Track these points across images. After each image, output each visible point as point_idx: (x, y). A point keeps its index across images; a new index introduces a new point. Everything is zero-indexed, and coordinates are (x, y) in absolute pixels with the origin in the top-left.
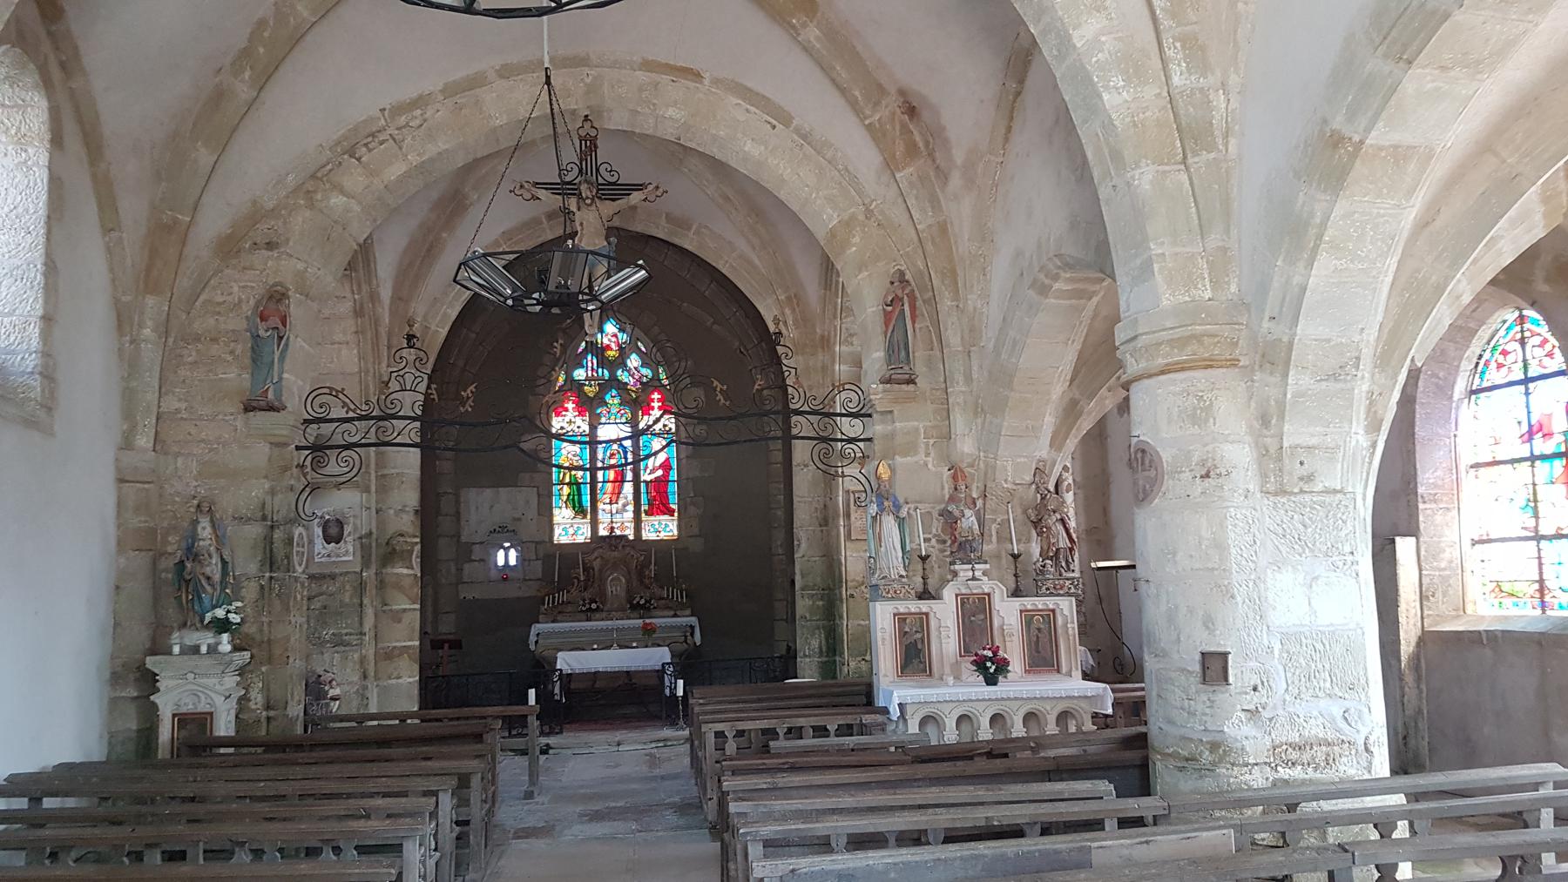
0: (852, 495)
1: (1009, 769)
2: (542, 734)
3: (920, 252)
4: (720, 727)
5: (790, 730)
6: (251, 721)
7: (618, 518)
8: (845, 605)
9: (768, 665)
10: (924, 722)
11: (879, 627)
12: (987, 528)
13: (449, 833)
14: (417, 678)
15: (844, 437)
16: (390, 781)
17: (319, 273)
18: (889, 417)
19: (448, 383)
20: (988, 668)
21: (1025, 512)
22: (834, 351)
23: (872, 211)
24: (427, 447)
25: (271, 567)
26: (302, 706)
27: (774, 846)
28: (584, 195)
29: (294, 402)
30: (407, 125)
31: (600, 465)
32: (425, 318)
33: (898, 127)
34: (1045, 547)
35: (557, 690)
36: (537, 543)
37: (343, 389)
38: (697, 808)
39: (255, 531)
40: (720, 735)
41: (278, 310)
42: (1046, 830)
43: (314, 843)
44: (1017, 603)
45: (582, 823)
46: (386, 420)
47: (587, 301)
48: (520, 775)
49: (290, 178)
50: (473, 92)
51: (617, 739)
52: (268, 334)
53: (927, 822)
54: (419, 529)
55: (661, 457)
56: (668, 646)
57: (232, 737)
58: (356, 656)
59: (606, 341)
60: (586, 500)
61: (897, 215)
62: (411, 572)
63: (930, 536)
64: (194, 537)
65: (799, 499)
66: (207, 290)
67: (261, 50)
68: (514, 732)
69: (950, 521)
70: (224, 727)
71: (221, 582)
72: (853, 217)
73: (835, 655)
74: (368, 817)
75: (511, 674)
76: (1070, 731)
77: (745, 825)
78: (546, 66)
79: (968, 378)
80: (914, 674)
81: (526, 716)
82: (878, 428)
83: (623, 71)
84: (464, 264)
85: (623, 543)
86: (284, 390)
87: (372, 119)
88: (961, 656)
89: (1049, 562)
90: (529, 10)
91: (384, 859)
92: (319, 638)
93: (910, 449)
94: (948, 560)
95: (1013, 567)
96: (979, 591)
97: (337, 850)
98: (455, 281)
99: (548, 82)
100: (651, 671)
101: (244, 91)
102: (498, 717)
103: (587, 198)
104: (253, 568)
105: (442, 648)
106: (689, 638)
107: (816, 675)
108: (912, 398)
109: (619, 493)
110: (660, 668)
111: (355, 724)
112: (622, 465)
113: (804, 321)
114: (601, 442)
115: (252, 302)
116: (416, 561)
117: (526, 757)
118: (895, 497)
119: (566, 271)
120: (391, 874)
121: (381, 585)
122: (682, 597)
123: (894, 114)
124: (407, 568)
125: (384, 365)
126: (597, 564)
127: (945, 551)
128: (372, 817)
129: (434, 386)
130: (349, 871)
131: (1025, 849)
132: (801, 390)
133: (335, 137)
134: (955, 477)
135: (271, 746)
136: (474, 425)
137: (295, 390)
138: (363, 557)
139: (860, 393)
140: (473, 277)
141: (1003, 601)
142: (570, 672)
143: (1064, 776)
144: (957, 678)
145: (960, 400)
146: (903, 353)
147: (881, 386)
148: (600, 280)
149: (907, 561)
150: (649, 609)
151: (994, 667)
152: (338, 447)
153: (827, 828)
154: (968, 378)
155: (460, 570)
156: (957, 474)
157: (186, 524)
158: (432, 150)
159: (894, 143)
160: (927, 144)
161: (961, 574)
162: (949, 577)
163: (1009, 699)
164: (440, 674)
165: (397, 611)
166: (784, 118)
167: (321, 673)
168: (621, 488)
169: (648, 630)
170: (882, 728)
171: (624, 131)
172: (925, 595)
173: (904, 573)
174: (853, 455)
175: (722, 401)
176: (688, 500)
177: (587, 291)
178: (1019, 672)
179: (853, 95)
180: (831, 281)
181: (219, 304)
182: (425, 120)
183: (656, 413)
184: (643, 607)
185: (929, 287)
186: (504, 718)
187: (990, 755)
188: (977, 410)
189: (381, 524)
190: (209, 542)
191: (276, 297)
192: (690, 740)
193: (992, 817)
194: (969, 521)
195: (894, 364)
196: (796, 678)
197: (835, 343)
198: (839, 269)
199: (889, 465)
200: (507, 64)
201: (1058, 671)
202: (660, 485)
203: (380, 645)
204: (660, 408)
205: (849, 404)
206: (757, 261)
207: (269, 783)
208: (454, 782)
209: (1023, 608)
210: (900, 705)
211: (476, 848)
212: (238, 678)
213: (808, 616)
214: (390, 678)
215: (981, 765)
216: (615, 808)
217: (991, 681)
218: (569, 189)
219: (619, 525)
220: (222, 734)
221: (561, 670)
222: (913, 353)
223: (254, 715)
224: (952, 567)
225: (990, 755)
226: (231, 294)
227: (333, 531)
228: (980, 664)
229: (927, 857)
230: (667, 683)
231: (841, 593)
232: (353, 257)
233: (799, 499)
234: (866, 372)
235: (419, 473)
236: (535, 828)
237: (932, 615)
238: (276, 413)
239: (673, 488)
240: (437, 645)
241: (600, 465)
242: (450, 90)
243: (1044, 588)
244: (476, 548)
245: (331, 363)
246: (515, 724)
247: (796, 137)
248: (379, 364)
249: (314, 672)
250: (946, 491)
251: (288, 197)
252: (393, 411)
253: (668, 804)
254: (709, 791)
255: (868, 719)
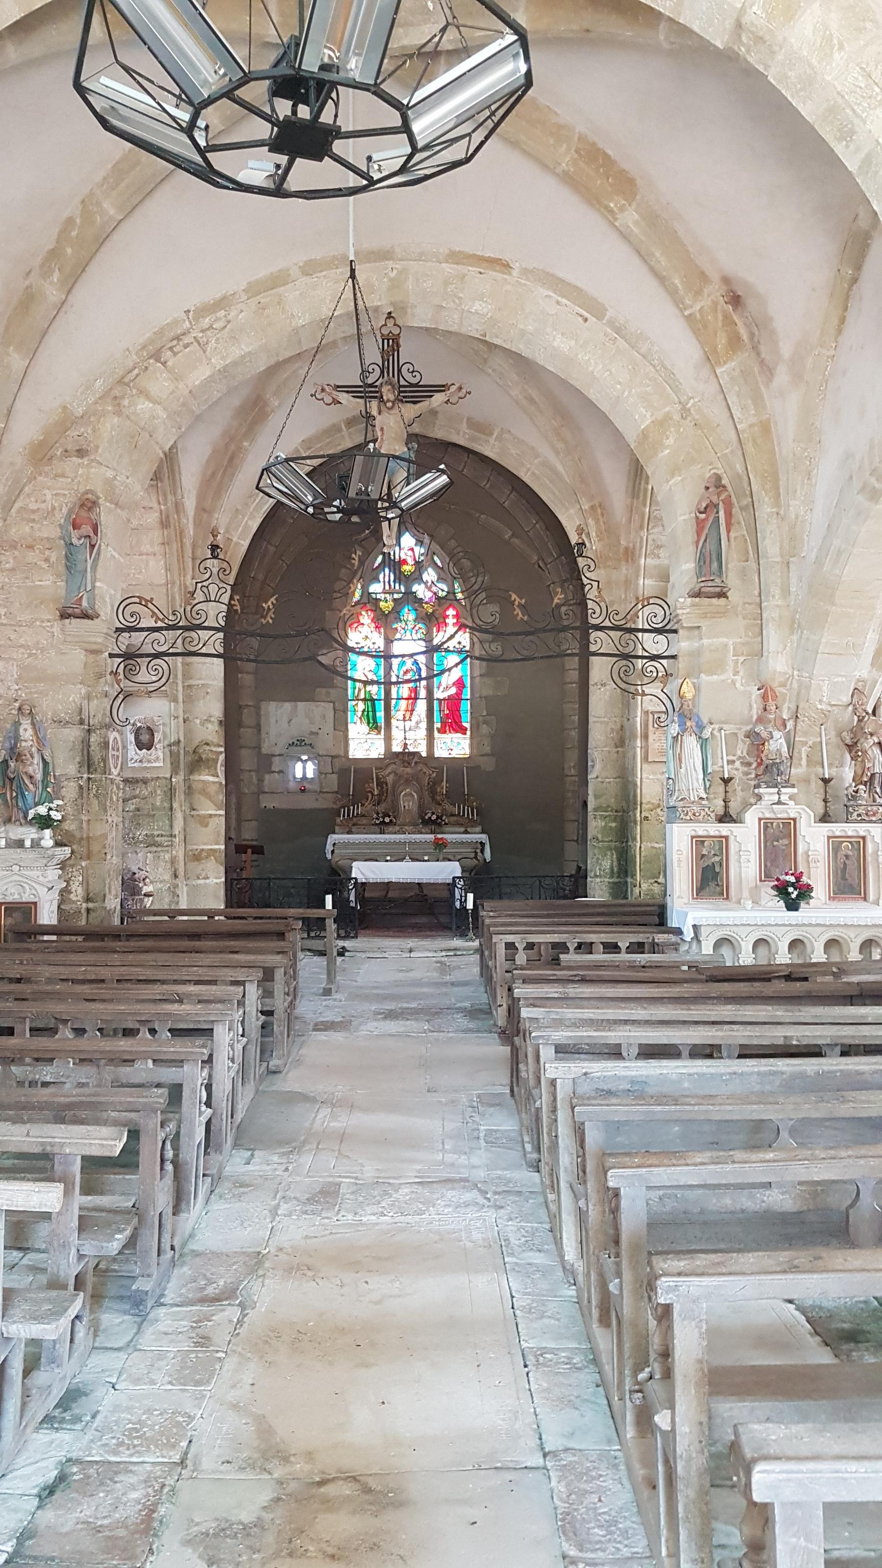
0: (651, 716)
1: (810, 992)
2: (339, 937)
3: (740, 453)
4: (510, 938)
5: (579, 946)
6: (72, 912)
7: (411, 735)
8: (638, 827)
9: (558, 884)
10: (718, 944)
11: (675, 848)
12: (796, 750)
13: (255, 1022)
14: (223, 880)
15: (647, 654)
16: (201, 971)
17: (128, 481)
18: (696, 632)
19: (249, 597)
20: (790, 894)
21: (839, 734)
22: (639, 566)
23: (689, 410)
24: (229, 657)
25: (89, 768)
26: (119, 900)
27: (563, 1051)
28: (385, 398)
29: (106, 610)
30: (211, 327)
31: (394, 679)
32: (227, 531)
33: (720, 318)
34: (860, 772)
35: (352, 898)
36: (333, 757)
37: (152, 599)
38: (487, 1013)
39: (74, 733)
40: (510, 946)
41: (90, 518)
42: (847, 1051)
43: (130, 1025)
44: (826, 829)
45: (377, 1020)
46: (192, 630)
47: (387, 509)
48: (319, 973)
49: (98, 383)
50: (274, 291)
51: (409, 946)
52: (81, 542)
53: (722, 1038)
54: (223, 740)
55: (456, 674)
56: (458, 861)
57: (54, 926)
58: (167, 856)
59: (403, 557)
60: (381, 715)
61: (716, 413)
62: (216, 779)
63: (734, 758)
64: (17, 738)
65: (595, 719)
66: (21, 498)
67: (69, 251)
68: (312, 934)
69: (757, 742)
70: (47, 916)
71: (43, 782)
72: (668, 417)
73: (627, 876)
74: (181, 1001)
75: (309, 880)
76: (873, 958)
77: (539, 1028)
78: (352, 258)
79: (786, 592)
80: (712, 895)
81: (325, 919)
82: (682, 644)
83: (430, 264)
84: (266, 470)
85: (416, 759)
86: (97, 598)
87: (176, 322)
88: (761, 880)
89: (862, 787)
90: (340, 190)
91: (199, 1041)
92: (133, 838)
93: (717, 667)
94: (753, 783)
95: (822, 791)
96: (785, 815)
97: (153, 1031)
98: (257, 488)
99: (353, 276)
100: (441, 884)
101: (52, 293)
102: (299, 919)
103: (388, 401)
104: (72, 769)
105: (246, 853)
106: (480, 854)
107: (607, 895)
108: (722, 613)
109: (413, 710)
110: (451, 881)
111: (166, 918)
112: (415, 681)
113: (609, 532)
114: (396, 657)
115: (65, 510)
116: (220, 770)
117: (324, 959)
118: (698, 717)
119: (366, 478)
120: (203, 1053)
121: (189, 791)
122: (473, 815)
123: (715, 303)
124: (213, 775)
125: (189, 577)
126: (390, 779)
127: (750, 774)
128: (185, 1001)
129: (237, 597)
130: (165, 1049)
131: (826, 1068)
132: (602, 604)
133: (141, 341)
134: (764, 697)
135: (90, 935)
136: (275, 637)
137: (107, 599)
138: (172, 764)
139: (666, 607)
140: (275, 484)
141: (810, 826)
142: (364, 881)
143: (867, 1002)
144: (756, 902)
145: (775, 615)
146: (715, 565)
147: (689, 600)
148: (399, 488)
149: (708, 784)
150: (440, 825)
151: (796, 893)
152: (148, 655)
153: (620, 1037)
154: (786, 592)
155: (261, 780)
156: (767, 694)
157: (8, 726)
158: (236, 352)
159: (716, 335)
160: (752, 335)
161: (766, 797)
162: (753, 800)
163: (810, 925)
164: (244, 876)
165: (204, 816)
166: (596, 309)
167: (136, 871)
168: (414, 704)
169: (440, 845)
170: (675, 947)
171: (427, 329)
172: (725, 818)
173: (704, 796)
174: (655, 674)
175: (520, 615)
176: (481, 719)
177: (385, 497)
178: (823, 898)
179: (673, 283)
180: (639, 488)
181: (34, 512)
182: (229, 322)
183: (451, 630)
184: (434, 822)
185: (748, 493)
186: (304, 920)
187: (788, 978)
188: (794, 626)
189: (188, 733)
190: (31, 743)
191: (88, 504)
192: (480, 951)
193: (792, 1037)
194: (777, 744)
195: (705, 576)
196: (586, 897)
197: (640, 556)
198: (649, 473)
199: (694, 683)
200: (311, 260)
201: (865, 899)
202: (454, 702)
203: (189, 847)
204: (454, 624)
205: (653, 619)
206: (560, 468)
207: (89, 968)
208: (260, 975)
209: (831, 834)
210: (694, 926)
211: (279, 1037)
212: (60, 872)
213: (600, 837)
214: (198, 878)
215: (780, 986)
216: (407, 1009)
217: (792, 906)
218: (371, 392)
219: (412, 741)
220: (46, 923)
221: (355, 878)
222: (727, 564)
223: (74, 906)
224: (756, 791)
225: (788, 978)
226: (45, 502)
227: (145, 738)
228: (782, 890)
229: (722, 1070)
230: (457, 896)
231: (635, 815)
232: (158, 466)
233: (595, 719)
234: (673, 586)
235: (222, 684)
236: (333, 1022)
237: (732, 839)
238: (90, 622)
239: (466, 707)
240: (241, 849)
241: (394, 679)
242: (255, 289)
243: (856, 813)
244: (276, 760)
245: (139, 574)
246: (314, 926)
247: (609, 330)
248: (184, 576)
249: (129, 870)
250: (754, 711)
251: (96, 403)
252: (198, 622)
253: (460, 1008)
254: (499, 998)
255: (660, 938)
